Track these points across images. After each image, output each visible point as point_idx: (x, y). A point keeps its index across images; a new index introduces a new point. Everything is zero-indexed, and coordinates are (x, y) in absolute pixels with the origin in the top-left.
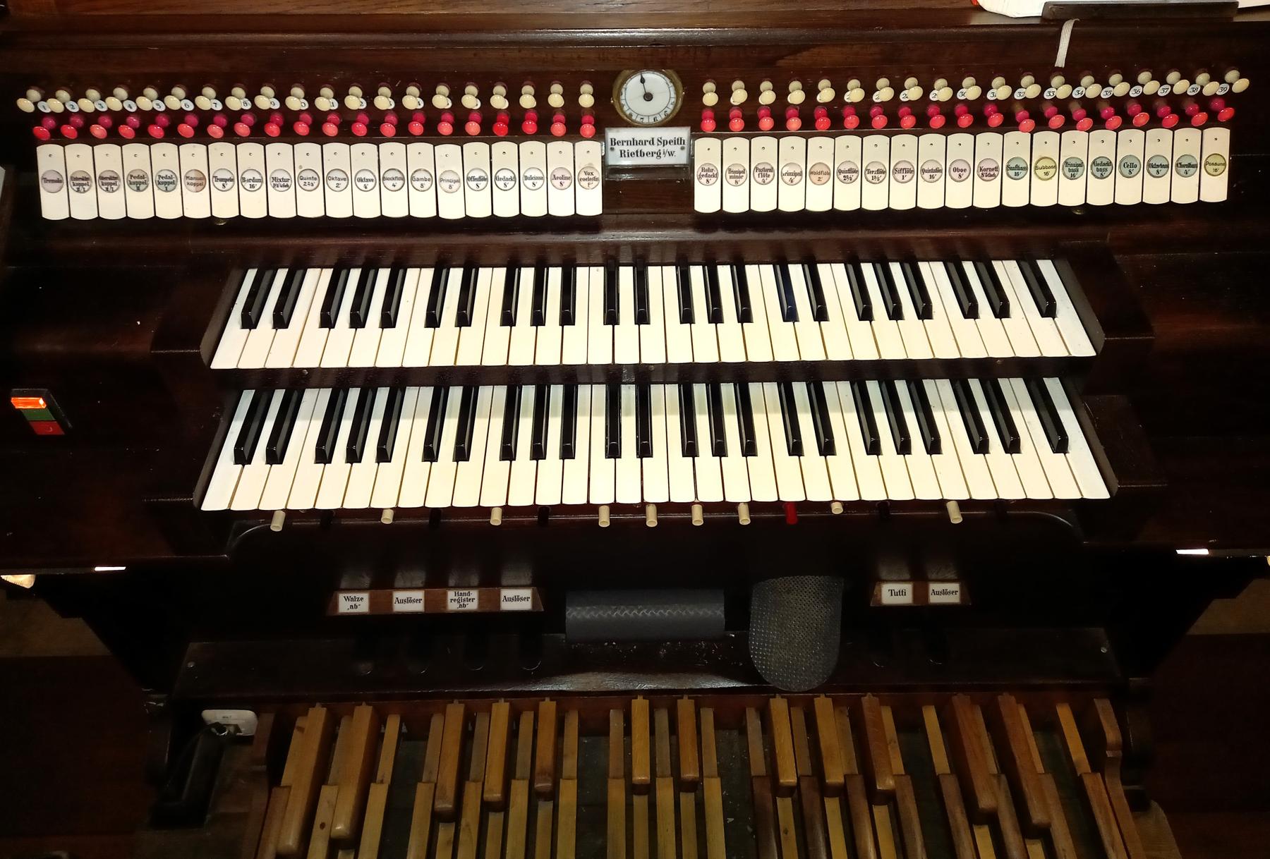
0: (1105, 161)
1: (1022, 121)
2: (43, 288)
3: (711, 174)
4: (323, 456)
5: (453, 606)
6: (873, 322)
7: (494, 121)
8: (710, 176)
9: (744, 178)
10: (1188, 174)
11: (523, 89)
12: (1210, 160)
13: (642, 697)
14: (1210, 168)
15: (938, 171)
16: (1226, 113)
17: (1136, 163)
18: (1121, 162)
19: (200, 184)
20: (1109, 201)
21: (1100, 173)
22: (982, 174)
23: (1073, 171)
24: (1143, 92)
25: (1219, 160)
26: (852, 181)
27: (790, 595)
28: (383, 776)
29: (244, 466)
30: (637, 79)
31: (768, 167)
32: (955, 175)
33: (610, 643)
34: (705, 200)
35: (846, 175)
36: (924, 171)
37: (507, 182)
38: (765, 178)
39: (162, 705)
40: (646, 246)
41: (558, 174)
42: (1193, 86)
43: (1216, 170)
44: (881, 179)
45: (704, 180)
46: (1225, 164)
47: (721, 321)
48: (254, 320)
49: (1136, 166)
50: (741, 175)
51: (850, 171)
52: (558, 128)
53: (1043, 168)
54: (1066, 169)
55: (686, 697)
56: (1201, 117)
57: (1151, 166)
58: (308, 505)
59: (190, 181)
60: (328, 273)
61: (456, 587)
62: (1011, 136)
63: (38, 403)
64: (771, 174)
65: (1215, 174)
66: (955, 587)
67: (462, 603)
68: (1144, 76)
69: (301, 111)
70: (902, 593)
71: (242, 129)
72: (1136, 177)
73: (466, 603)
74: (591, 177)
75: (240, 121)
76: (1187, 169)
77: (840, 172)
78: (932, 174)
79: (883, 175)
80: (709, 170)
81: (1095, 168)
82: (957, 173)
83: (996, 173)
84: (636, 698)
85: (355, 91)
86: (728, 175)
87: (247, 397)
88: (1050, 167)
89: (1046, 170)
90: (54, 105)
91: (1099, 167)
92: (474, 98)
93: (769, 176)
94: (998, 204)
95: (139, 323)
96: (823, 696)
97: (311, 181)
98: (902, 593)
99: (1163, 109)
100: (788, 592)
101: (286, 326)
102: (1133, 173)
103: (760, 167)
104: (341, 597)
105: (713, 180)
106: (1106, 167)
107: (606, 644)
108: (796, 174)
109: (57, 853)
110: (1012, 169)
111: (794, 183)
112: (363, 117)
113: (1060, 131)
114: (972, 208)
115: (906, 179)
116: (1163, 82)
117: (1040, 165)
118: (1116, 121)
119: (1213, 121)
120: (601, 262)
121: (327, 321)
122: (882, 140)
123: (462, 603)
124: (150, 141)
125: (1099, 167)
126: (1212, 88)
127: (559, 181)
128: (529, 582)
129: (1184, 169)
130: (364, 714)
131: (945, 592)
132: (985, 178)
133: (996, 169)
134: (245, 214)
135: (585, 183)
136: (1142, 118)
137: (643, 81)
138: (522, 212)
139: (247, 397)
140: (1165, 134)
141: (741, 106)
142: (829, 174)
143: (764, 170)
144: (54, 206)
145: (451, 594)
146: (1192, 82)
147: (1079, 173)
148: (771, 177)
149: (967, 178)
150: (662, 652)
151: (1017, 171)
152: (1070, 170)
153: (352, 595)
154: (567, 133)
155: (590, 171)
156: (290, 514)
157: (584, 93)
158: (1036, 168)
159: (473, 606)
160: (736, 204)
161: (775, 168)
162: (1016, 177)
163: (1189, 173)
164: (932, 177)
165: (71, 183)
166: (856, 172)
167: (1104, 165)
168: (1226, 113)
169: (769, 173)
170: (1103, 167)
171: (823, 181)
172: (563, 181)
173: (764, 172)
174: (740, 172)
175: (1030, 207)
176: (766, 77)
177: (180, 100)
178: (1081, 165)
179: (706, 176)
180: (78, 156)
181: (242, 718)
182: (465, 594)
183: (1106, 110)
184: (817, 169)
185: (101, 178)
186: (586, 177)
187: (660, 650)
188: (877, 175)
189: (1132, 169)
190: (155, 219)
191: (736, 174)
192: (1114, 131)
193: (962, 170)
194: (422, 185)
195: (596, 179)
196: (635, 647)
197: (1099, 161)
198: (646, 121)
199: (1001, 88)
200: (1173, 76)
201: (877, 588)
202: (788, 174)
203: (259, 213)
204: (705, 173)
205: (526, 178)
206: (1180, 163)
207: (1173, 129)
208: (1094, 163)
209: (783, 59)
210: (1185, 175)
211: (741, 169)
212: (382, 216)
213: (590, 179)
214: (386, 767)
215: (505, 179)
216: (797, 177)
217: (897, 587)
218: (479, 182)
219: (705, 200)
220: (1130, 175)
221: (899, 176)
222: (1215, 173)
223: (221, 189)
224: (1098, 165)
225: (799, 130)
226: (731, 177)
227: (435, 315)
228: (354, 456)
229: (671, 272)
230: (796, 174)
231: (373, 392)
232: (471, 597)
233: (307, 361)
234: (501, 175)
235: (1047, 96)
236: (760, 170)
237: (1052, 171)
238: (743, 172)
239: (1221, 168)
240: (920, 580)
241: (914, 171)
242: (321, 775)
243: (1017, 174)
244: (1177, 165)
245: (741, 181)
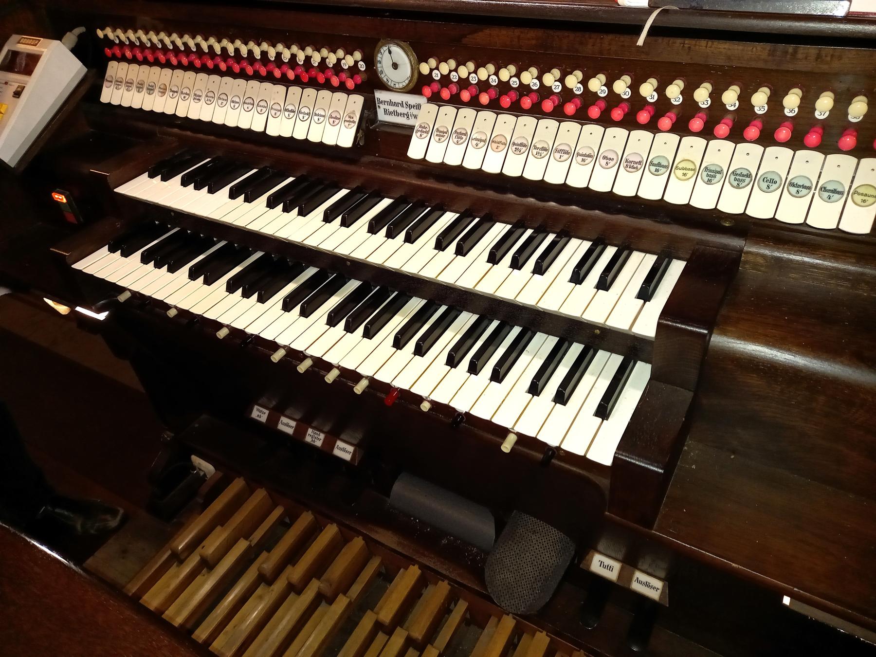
0: (745, 173)
2: (91, 141)
3: (424, 130)
4: (535, 389)
5: (308, 439)
7: (747, 124)
8: (423, 132)
9: (445, 137)
11: (531, 68)
13: (418, 566)
14: (858, 198)
15: (590, 156)
17: (777, 179)
19: (164, 93)
21: (737, 182)
22: (627, 165)
23: (711, 176)
27: (534, 535)
28: (253, 539)
29: (451, 368)
30: (385, 48)
32: (603, 162)
33: (415, 519)
34: (415, 151)
35: (517, 147)
36: (578, 154)
37: (304, 115)
38: (459, 140)
39: (169, 439)
43: (864, 201)
44: (543, 155)
45: (419, 134)
48: (497, 259)
49: (776, 182)
51: (522, 145)
54: (705, 174)
55: (446, 582)
58: (486, 416)
59: (160, 90)
61: (314, 428)
63: (62, 199)
64: (464, 137)
66: (659, 584)
67: (314, 439)
70: (610, 568)
72: (807, 196)
73: (316, 440)
74: (352, 120)
76: (831, 194)
77: (514, 144)
78: (584, 158)
79: (545, 153)
80: (424, 127)
81: (733, 177)
82: (605, 161)
83: (639, 166)
84: (414, 565)
87: (415, 304)
88: (689, 169)
89: (685, 172)
90: (463, 72)
91: (738, 177)
96: (545, 633)
97: (211, 99)
98: (610, 568)
100: (534, 532)
102: (772, 188)
104: (256, 407)
105: (425, 135)
106: (744, 178)
107: (412, 518)
108: (481, 141)
109: (119, 508)
110: (654, 165)
114: (542, 181)
115: (563, 159)
117: (680, 166)
121: (577, 278)
123: (314, 439)
125: (738, 177)
127: (333, 119)
128: (355, 442)
129: (828, 194)
130: (260, 495)
131: (647, 585)
132: (628, 169)
133: (640, 163)
134: (213, 121)
135: (347, 124)
137: (390, 52)
139: (415, 304)
144: (105, 98)
145: (310, 431)
148: (445, 137)
149: (691, 177)
150: (444, 541)
151: (658, 168)
152: (708, 175)
153: (261, 409)
155: (352, 116)
156: (374, 383)
159: (319, 444)
160: (434, 157)
161: (469, 134)
163: (832, 199)
164: (583, 160)
165: (435, 133)
166: (525, 146)
167: (744, 176)
172: (335, 120)
173: (460, 135)
174: (444, 132)
179: (422, 131)
180: (135, 72)
181: (206, 467)
182: (317, 434)
184: (498, 139)
186: (348, 119)
187: (442, 540)
188: (540, 152)
189: (771, 184)
191: (441, 134)
193: (610, 159)
194: (261, 110)
195: (354, 122)
196: (429, 530)
197: (739, 172)
198: (397, 86)
201: (591, 553)
202: (476, 139)
204: (421, 129)
205: (316, 115)
206: (825, 188)
208: (733, 172)
209: (466, 37)
211: (445, 130)
212: (306, 140)
213: (350, 121)
214: (356, 589)
215: (304, 113)
217: (608, 561)
218: (290, 113)
219: (415, 151)
221: (557, 155)
223: (605, 166)
226: (437, 135)
228: (474, 369)
230: (481, 141)
231: (569, 344)
232: (320, 437)
233: (466, 283)
234: (303, 110)
240: (630, 562)
241: (340, 118)
242: (221, 519)
243: (657, 170)
245: (443, 139)
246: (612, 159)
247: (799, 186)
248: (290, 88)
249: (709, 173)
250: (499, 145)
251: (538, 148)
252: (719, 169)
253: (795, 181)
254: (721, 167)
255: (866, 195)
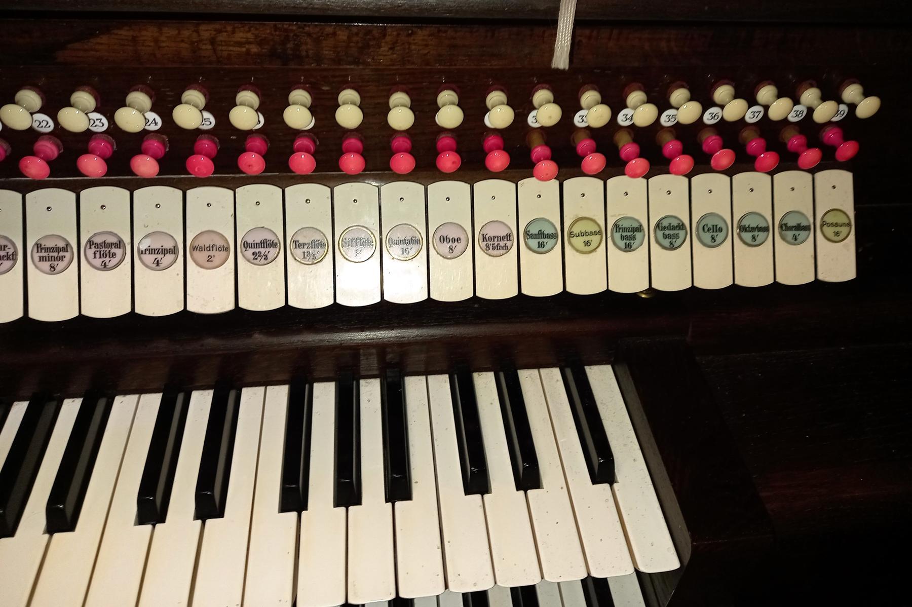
1: (539, 161)
6: (615, 485)
7: (389, 152)
9: (66, 260)
10: (798, 241)
12: (829, 219)
14: (829, 231)
16: (847, 150)
17: (721, 224)
18: (698, 223)
20: (600, 288)
22: (487, 246)
24: (722, 117)
25: (842, 219)
26: (316, 261)
31: (112, 240)
32: (445, 248)
35: (257, 250)
38: (107, 259)
40: (402, 346)
41: (792, 222)
42: (797, 108)
46: (849, 225)
47: (358, 501)
49: (721, 230)
50: (61, 254)
52: (303, 161)
53: (582, 234)
54: (617, 236)
56: (811, 156)
57: (743, 229)
60: (152, 402)
62: (528, 185)
64: (119, 252)
65: (837, 239)
68: (722, 92)
69: (198, 132)
71: (201, 164)
75: (244, 150)
76: (797, 233)
81: (660, 234)
83: (509, 244)
85: (345, 97)
86: (36, 256)
88: (591, 234)
89: (586, 238)
91: (667, 232)
92: (196, 112)
93: (114, 255)
94: (515, 293)
95: (893, 451)
99: (754, 144)
101: (220, 513)
102: (719, 240)
103: (98, 240)
106: (676, 232)
108: (165, 252)
110: (532, 236)
111: (162, 266)
112: (258, 143)
113: (604, 176)
116: (752, 101)
117: (576, 229)
118: (684, 162)
119: (828, 162)
120: (331, 375)
122: (504, 187)
124: (133, 184)
125: (667, 232)
126: (825, 112)
132: (491, 251)
133: (508, 237)
134: (781, 280)
136: (724, 157)
138: (431, 297)
140: (719, 181)
141: (455, 132)
142: (227, 249)
143: (105, 244)
146: (796, 102)
147: (637, 242)
151: (541, 241)
152: (623, 238)
154: (511, 166)
157: (294, 104)
158: (571, 234)
161: (127, 240)
162: (541, 249)
163: (800, 239)
165: (434, 242)
166: (273, 245)
167: (674, 228)
168: (847, 150)
169: (113, 250)
170: (672, 232)
171: (216, 261)
174: (58, 250)
175: (565, 296)
176: (584, 84)
177: (32, 114)
178: (639, 229)
183: (671, 145)
184: (205, 241)
185: (246, 245)
188: (311, 250)
189: (715, 234)
190: (693, 290)
192: (768, 173)
193: (454, 240)
199: (594, 109)
200: (766, 93)
202: (151, 251)
203: (220, 304)
206: (786, 225)
207: (772, 174)
210: (793, 241)
216: (168, 256)
220: (713, 243)
222: (836, 238)
224: (665, 228)
225: (103, 176)
226: (42, 259)
227: (212, 497)
229: (441, 385)
230: (165, 252)
235: (622, 120)
236: (97, 246)
237: (595, 239)
238: (65, 249)
239: (844, 230)
243: (541, 245)
244: (781, 227)
245: (61, 265)
246: (458, 240)
247: (753, 229)
248: (609, 181)
249: (624, 234)
250: (211, 253)
251: (304, 244)
252: (636, 225)
253: (745, 223)
254: (637, 221)
255: (836, 225)
